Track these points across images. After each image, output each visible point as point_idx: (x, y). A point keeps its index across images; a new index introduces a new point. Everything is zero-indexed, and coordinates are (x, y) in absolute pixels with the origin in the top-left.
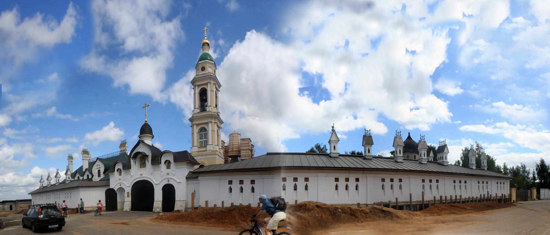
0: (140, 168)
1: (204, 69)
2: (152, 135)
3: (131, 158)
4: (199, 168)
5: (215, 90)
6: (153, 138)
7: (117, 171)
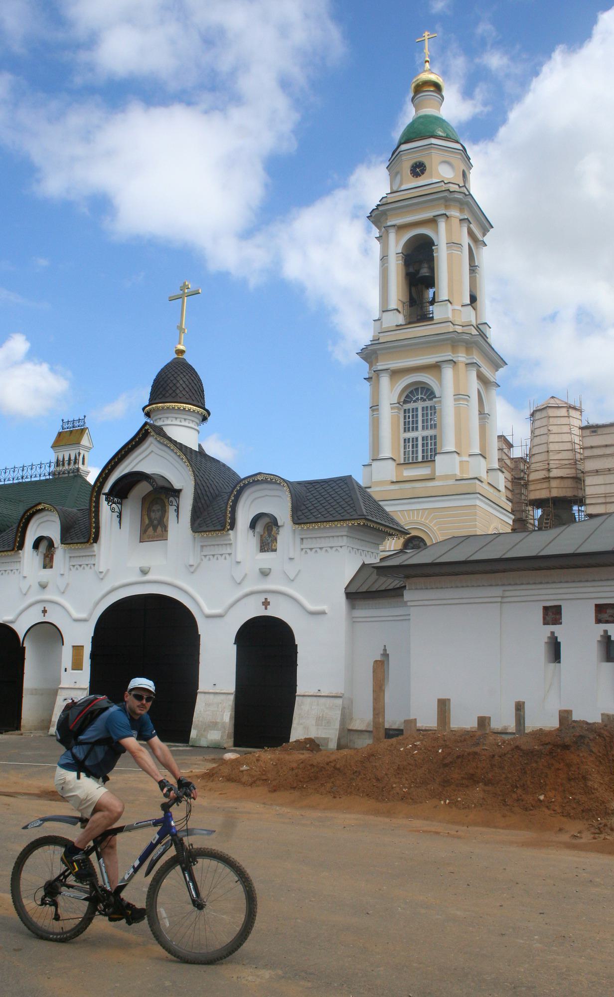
0: (142, 541)
2: (204, 409)
3: (103, 497)
4: (401, 551)
5: (466, 240)
6: (204, 419)
7: (36, 546)
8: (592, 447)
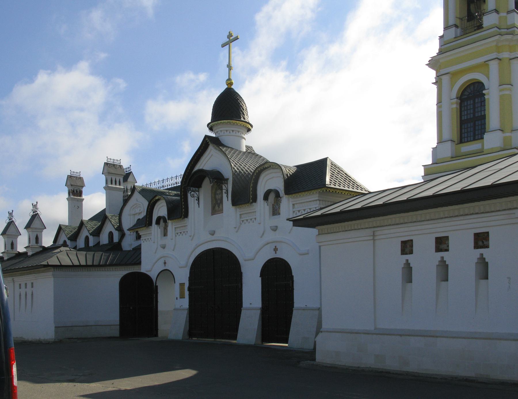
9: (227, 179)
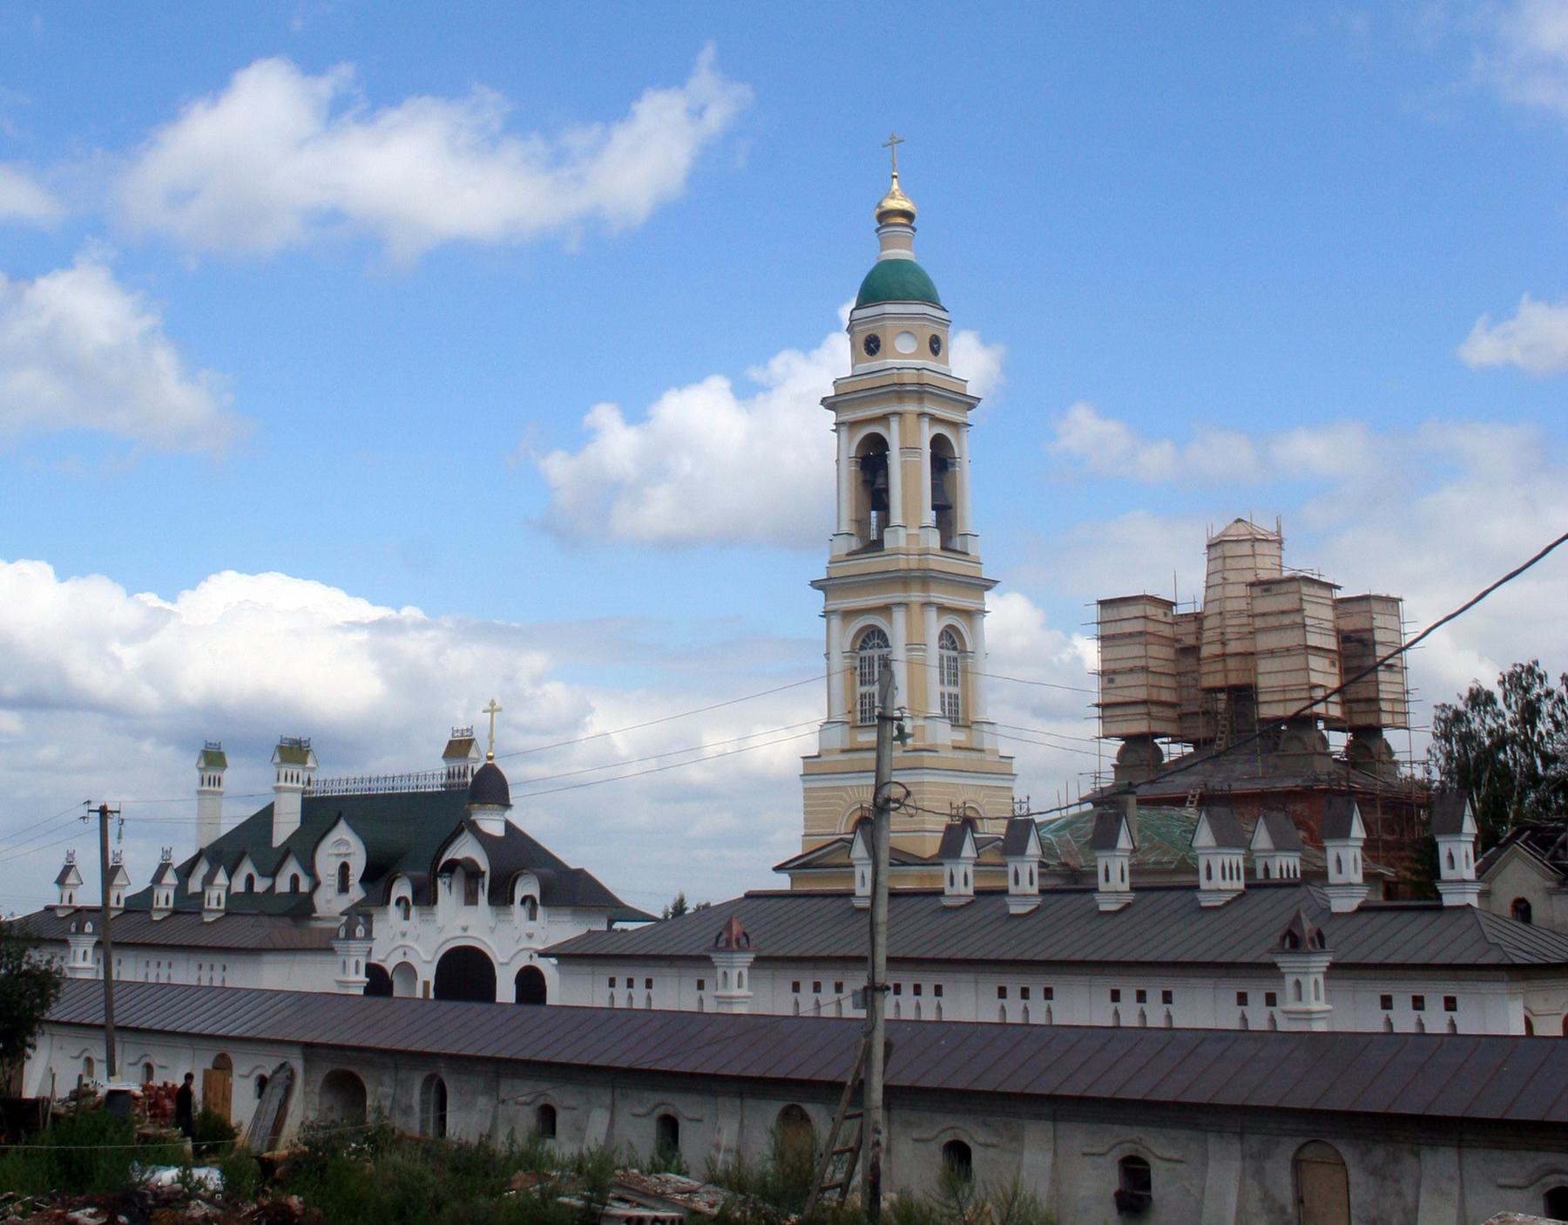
1: (878, 347)
8: (1264, 615)
9: (484, 873)
